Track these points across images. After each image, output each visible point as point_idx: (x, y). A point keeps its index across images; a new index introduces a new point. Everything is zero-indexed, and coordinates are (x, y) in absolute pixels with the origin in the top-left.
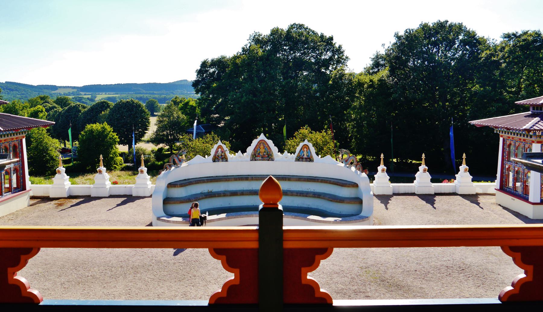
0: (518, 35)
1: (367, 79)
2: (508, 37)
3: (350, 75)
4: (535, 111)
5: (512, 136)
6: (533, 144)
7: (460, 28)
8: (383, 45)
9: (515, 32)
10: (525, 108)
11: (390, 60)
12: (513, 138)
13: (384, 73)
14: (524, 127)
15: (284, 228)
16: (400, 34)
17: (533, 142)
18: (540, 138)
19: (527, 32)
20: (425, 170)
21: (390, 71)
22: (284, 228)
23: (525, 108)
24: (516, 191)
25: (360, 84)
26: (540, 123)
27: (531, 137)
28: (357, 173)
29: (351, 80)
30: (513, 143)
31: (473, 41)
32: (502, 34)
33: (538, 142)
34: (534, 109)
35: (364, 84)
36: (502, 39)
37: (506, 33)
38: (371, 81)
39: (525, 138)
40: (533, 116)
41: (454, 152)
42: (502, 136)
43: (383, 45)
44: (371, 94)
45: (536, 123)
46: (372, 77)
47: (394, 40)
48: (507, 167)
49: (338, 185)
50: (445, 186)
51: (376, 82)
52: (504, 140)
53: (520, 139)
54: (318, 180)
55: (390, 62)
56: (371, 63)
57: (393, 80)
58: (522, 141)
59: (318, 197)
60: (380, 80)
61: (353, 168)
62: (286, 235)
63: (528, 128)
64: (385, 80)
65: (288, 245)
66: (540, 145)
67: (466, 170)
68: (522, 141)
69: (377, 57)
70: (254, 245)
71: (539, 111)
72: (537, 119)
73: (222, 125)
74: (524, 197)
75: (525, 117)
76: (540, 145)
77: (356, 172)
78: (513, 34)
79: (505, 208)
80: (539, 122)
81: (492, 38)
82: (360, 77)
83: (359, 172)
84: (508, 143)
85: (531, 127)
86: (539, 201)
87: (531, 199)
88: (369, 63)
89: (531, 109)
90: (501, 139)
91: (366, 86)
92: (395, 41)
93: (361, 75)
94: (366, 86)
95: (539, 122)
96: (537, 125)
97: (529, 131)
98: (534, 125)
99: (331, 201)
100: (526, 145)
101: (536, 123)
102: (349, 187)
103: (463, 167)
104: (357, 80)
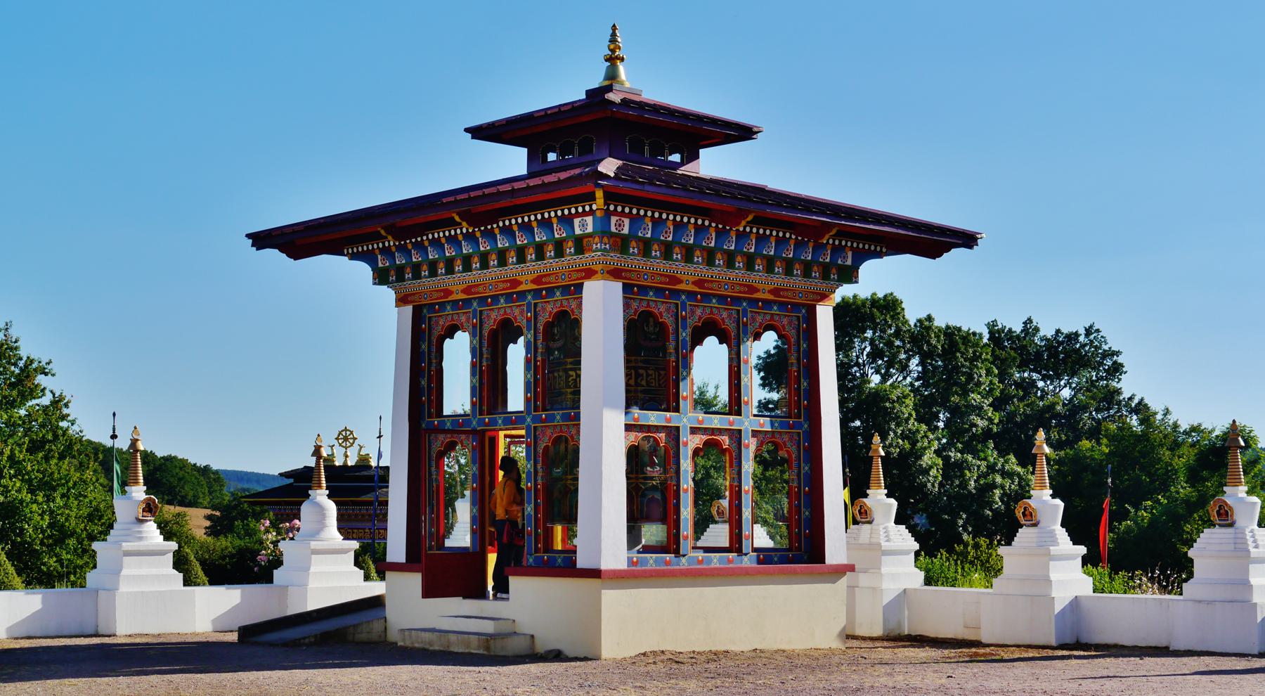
17: (590, 274)
33: (615, 274)
66: (617, 286)
76: (617, 286)
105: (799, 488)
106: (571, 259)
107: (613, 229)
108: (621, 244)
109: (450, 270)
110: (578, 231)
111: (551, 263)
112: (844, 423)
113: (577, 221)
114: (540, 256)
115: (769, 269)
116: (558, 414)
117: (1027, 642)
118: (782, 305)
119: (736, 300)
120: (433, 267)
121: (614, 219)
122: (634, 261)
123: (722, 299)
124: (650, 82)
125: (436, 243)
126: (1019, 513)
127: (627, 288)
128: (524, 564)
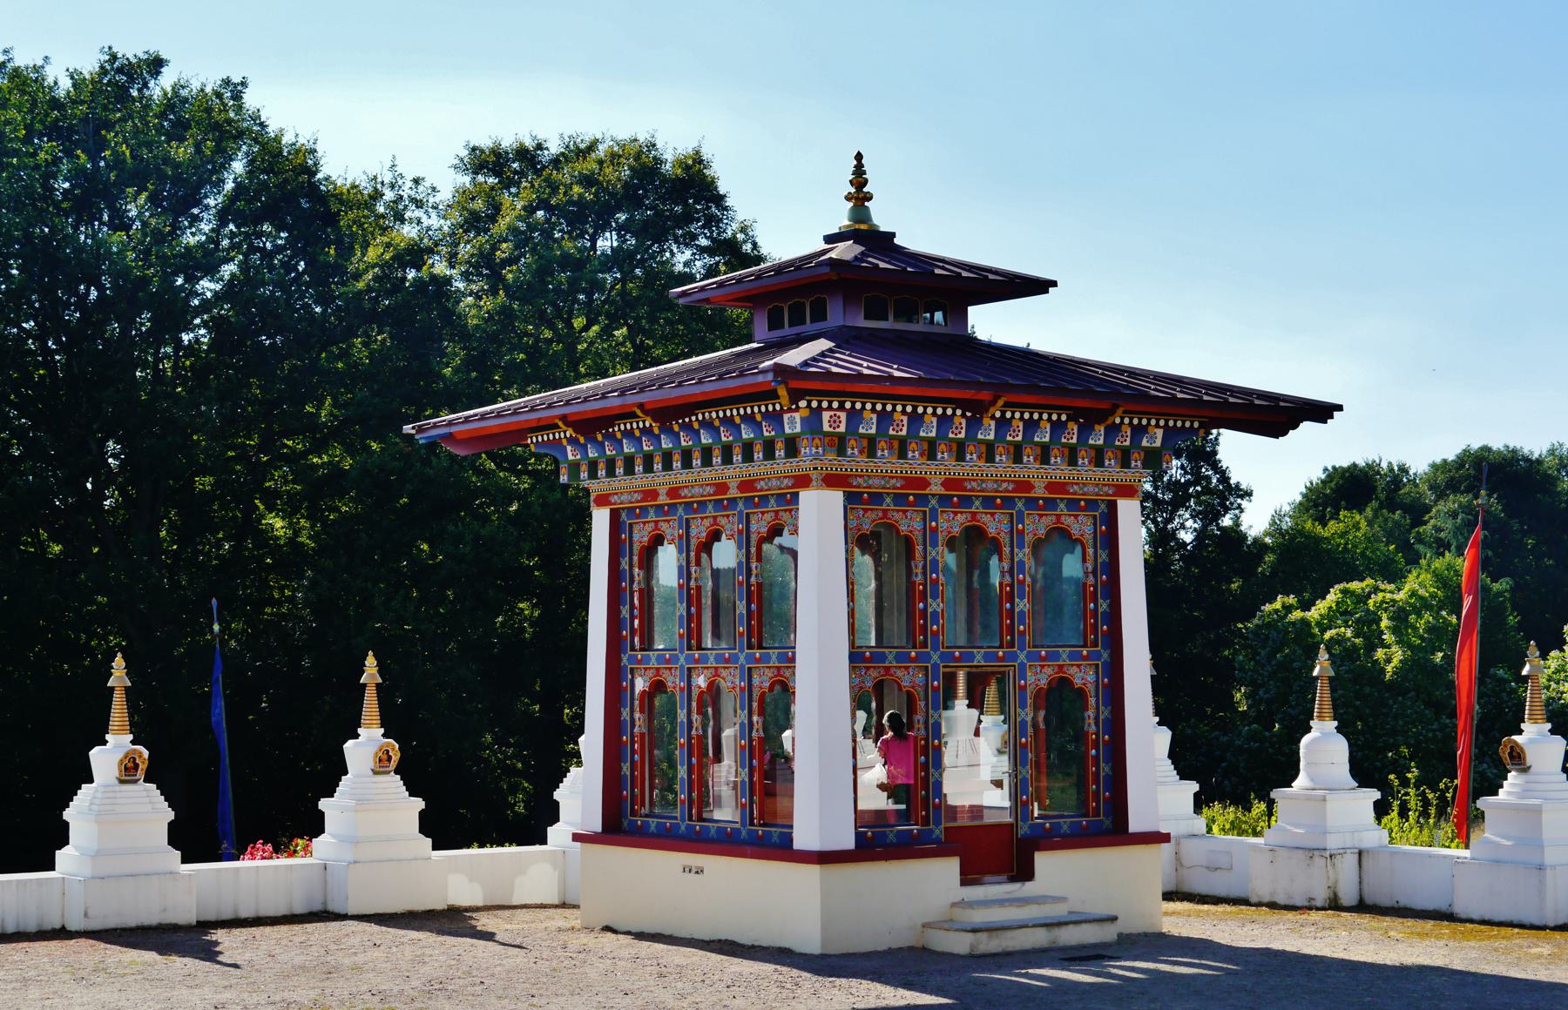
0: (545, 157)
2: (497, 173)
7: (218, 120)
9: (529, 143)
17: (803, 481)
19: (592, 146)
20: (128, 771)
31: (291, 192)
32: (464, 153)
33: (831, 481)
36: (465, 180)
37: (485, 143)
41: (231, 795)
42: (603, 501)
48: (640, 685)
50: (257, 876)
52: (615, 516)
66: (836, 497)
67: (383, 759)
74: (765, 836)
76: (836, 497)
78: (522, 153)
79: (641, 936)
81: (409, 177)
84: (641, 535)
86: (849, 843)
87: (803, 839)
90: (600, 520)
103: (365, 746)
105: (1097, 734)
106: (782, 465)
107: (826, 428)
108: (839, 444)
109: (727, 459)
110: (787, 431)
111: (759, 467)
112: (580, 717)
113: (786, 417)
114: (748, 457)
115: (1044, 458)
116: (774, 653)
117: (281, 911)
118: (1073, 504)
119: (1008, 502)
120: (707, 454)
121: (826, 416)
122: (855, 461)
123: (988, 502)
124: (924, 226)
125: (707, 425)
126: (1504, 753)
127: (851, 499)
128: (1008, 819)
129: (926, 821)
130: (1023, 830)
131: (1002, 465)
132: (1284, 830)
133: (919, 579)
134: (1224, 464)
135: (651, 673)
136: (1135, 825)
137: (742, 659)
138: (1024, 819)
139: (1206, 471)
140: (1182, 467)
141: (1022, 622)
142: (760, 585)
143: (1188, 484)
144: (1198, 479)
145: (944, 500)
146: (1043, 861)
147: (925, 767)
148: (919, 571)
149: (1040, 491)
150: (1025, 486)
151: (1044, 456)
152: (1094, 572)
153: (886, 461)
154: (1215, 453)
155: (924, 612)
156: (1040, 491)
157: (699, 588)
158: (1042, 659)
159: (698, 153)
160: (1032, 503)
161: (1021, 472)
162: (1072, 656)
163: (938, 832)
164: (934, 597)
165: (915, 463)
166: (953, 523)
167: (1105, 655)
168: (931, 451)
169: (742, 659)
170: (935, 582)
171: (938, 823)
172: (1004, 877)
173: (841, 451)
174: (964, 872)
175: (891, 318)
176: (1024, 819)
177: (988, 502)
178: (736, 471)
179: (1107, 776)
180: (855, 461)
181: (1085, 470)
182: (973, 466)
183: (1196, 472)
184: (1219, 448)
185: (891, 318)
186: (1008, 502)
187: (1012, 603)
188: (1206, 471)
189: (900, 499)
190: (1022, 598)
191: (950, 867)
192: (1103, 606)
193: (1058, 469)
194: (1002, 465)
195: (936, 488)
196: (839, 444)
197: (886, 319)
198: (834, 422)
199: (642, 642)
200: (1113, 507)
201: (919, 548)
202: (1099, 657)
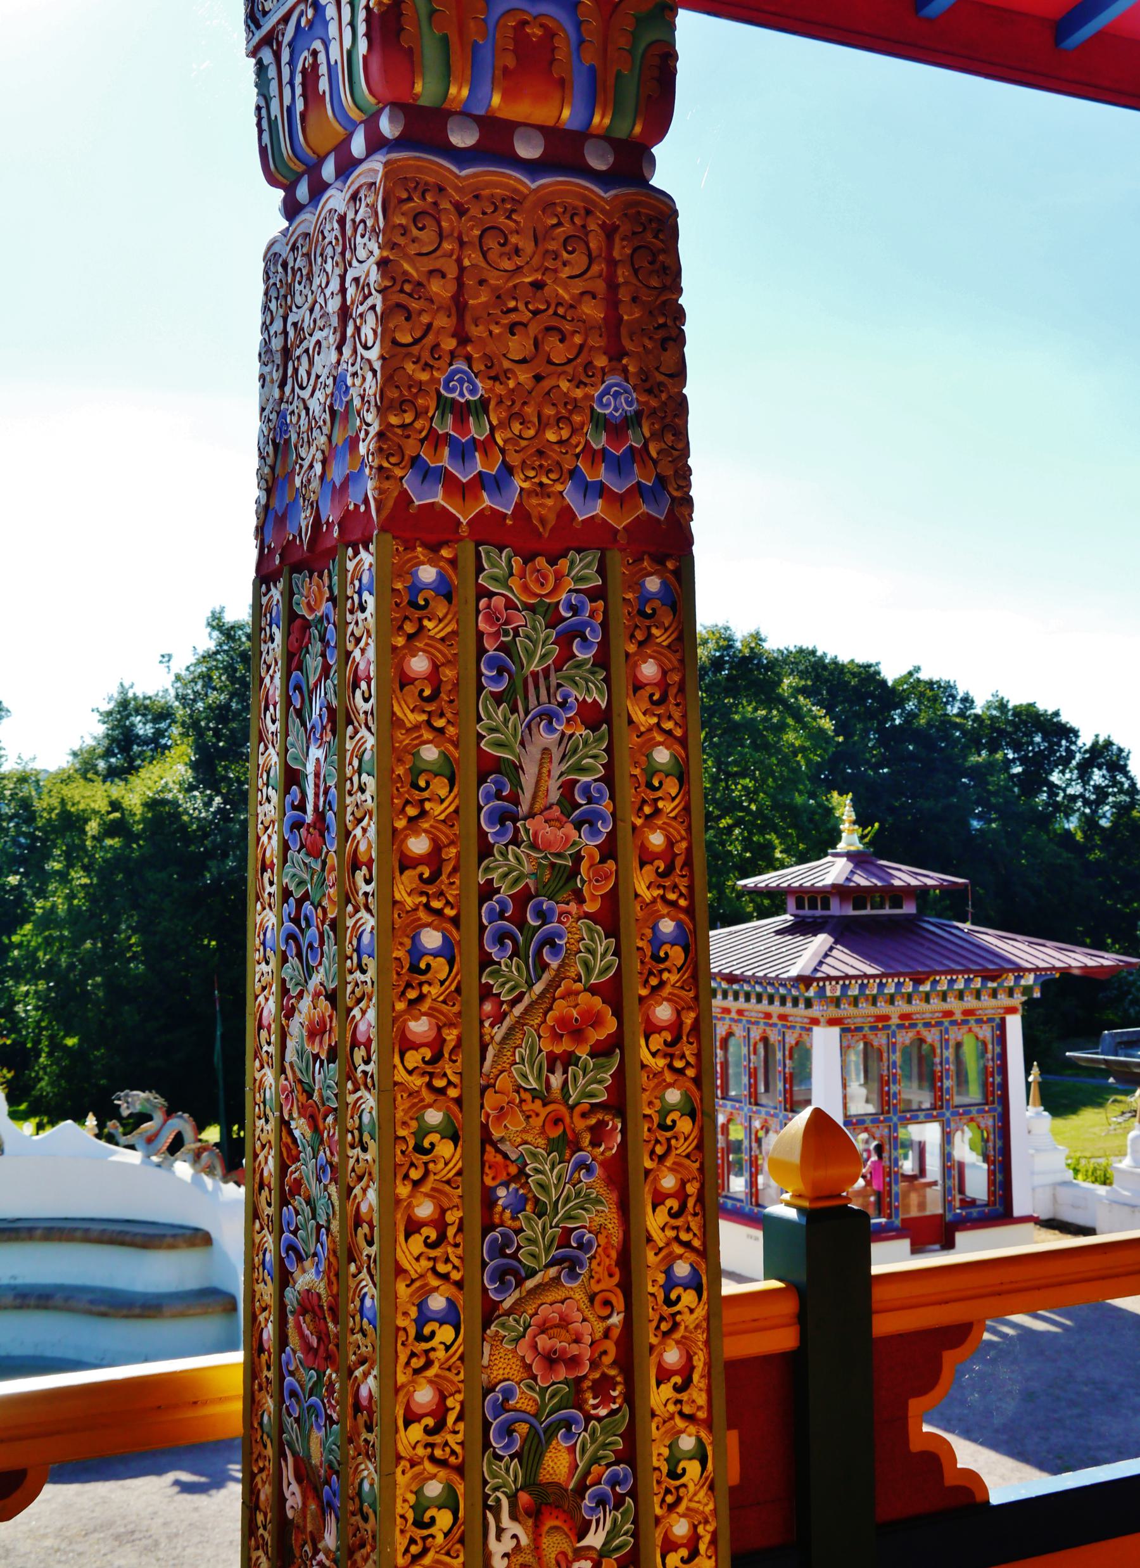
1: (94, 797)
3: (23, 779)
4: (806, 912)
5: (741, 1004)
6: (816, 1029)
8: (167, 658)
10: (771, 902)
11: (195, 724)
12: (740, 1012)
13: (169, 774)
14: (794, 972)
15: (876, 1270)
16: (229, 618)
17: (815, 1022)
18: (838, 1005)
21: (194, 766)
22: (876, 1270)
23: (771, 902)
24: (758, 1205)
25: (70, 822)
26: (835, 953)
27: (809, 1004)
28: (202, 1186)
29: (26, 804)
30: (738, 1030)
33: (832, 1022)
34: (800, 906)
35: (86, 821)
38: (115, 806)
39: (788, 1009)
40: (803, 928)
43: (167, 658)
44: (118, 861)
45: (826, 955)
46: (117, 790)
47: (208, 642)
49: (122, 1243)
51: (139, 810)
53: (768, 1016)
54: (31, 1230)
55: (193, 726)
56: (101, 729)
57: (208, 804)
58: (775, 1020)
59: (38, 1307)
60: (153, 804)
61: (183, 1169)
62: (879, 1294)
63: (808, 972)
64: (175, 803)
65: (884, 1325)
66: (836, 1031)
68: (775, 1020)
69: (124, 704)
70: (785, 1340)
71: (819, 912)
72: (822, 940)
73: (99, 979)
75: (778, 932)
76: (836, 1031)
77: (196, 1180)
80: (831, 949)
82: (67, 791)
83: (208, 1181)
85: (816, 970)
88: (91, 731)
89: (791, 904)
91: (93, 827)
92: (212, 646)
93: (67, 780)
94: (93, 827)
95: (831, 949)
96: (829, 960)
97: (805, 981)
98: (821, 963)
99: (104, 1315)
100: (788, 1033)
101: (826, 955)
102: (172, 1247)
104: (55, 802)
107: (828, 993)
119: (939, 1024)
122: (846, 1010)
123: (927, 1025)
129: (889, 1216)
130: (949, 1217)
131: (936, 1004)
132: (1117, 1191)
133: (885, 1073)
134: (1132, 774)
135: (727, 1114)
136: (1017, 1212)
137: (781, 1116)
138: (950, 1211)
139: (1120, 777)
140: (1104, 776)
141: (948, 1093)
142: (791, 1074)
143: (1107, 786)
144: (1115, 783)
145: (900, 1026)
146: (960, 1237)
147: (889, 1184)
148: (885, 1068)
149: (958, 1017)
150: (949, 1014)
151: (961, 995)
152: (993, 1059)
153: (865, 1008)
154: (1126, 765)
155: (888, 1093)
156: (958, 1017)
157: (755, 1069)
158: (961, 1115)
159: (758, 633)
160: (954, 1023)
161: (946, 1006)
162: (979, 1112)
163: (897, 1222)
164: (894, 1083)
165: (883, 1008)
166: (905, 1038)
167: (1000, 1109)
168: (891, 1000)
169: (781, 1116)
170: (895, 1075)
171: (897, 1216)
172: (937, 1247)
173: (838, 1005)
174: (912, 1244)
175: (869, 907)
176: (950, 1211)
177: (927, 1025)
178: (776, 1009)
179: (1000, 1196)
180: (846, 1010)
181: (987, 1002)
182: (918, 1006)
183: (1113, 777)
184: (1129, 762)
185: (869, 907)
186: (939, 1024)
187: (942, 1081)
188: (1120, 777)
189: (872, 1028)
190: (947, 1079)
191: (905, 1244)
192: (998, 1079)
193: (970, 1002)
194: (936, 1004)
195: (895, 1021)
196: (837, 1002)
197: (865, 908)
198: (833, 990)
199: (722, 1093)
200: (1003, 1020)
201: (885, 1055)
202: (995, 1110)
